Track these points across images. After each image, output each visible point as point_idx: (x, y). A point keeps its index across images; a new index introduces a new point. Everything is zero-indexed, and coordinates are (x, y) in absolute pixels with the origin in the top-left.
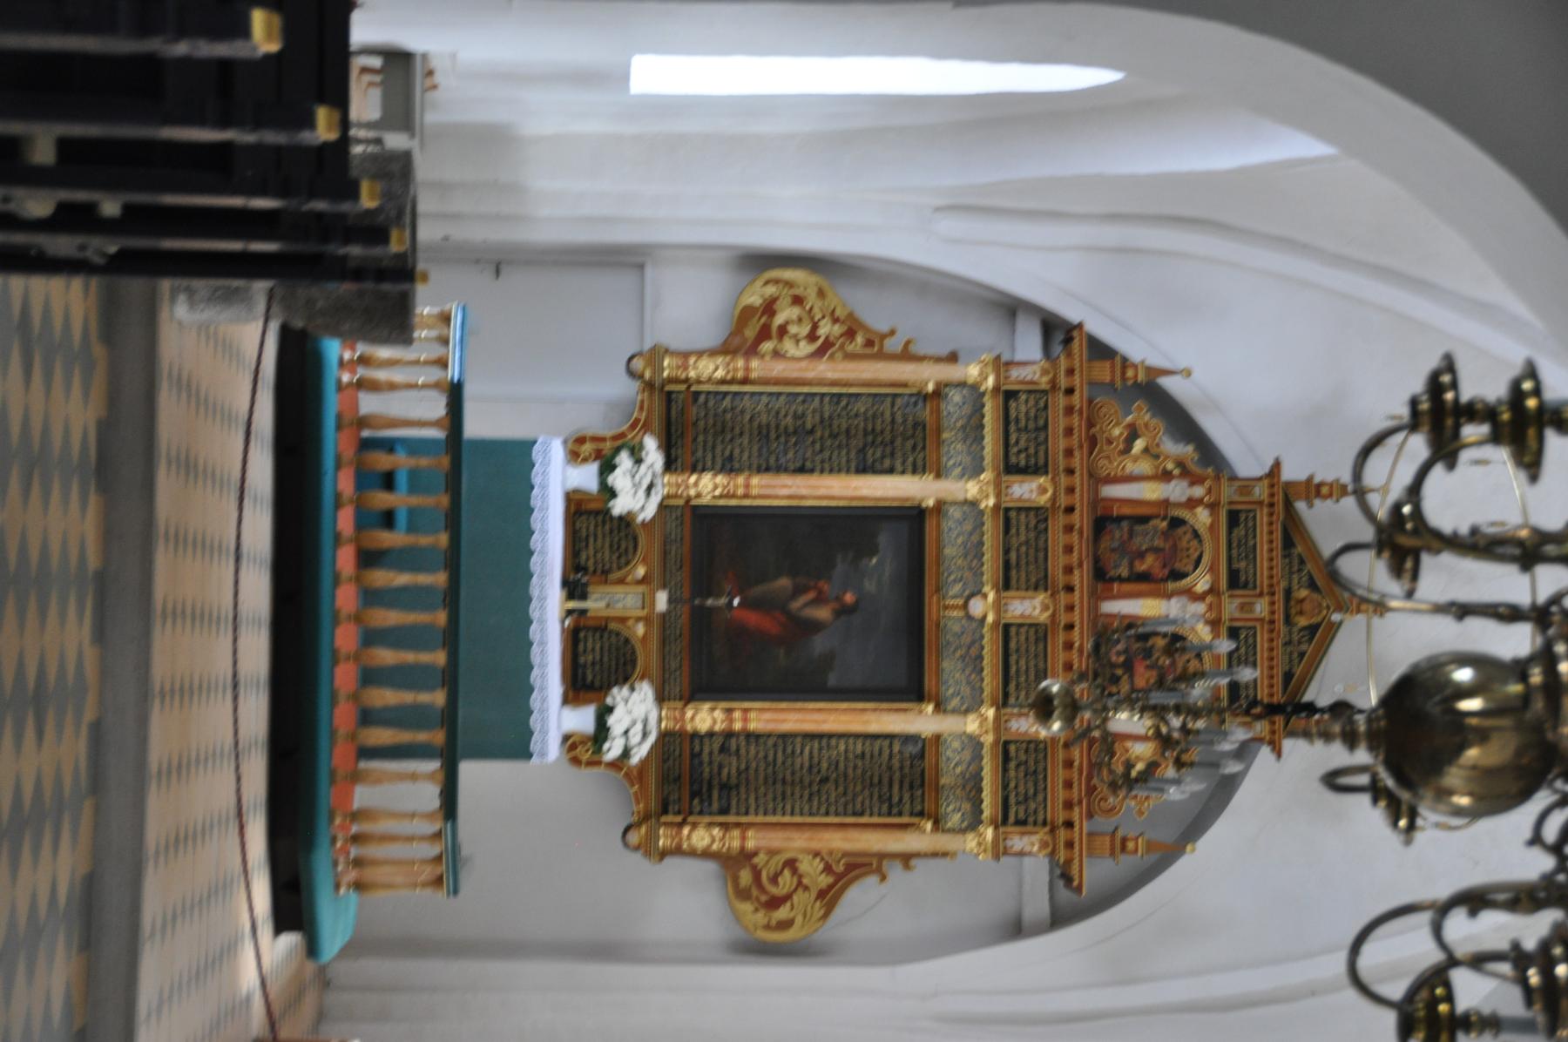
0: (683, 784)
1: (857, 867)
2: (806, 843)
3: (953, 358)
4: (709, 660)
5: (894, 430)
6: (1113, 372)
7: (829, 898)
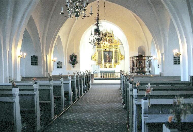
0: (116, 62)
1: (121, 54)
2: (119, 56)
3: (96, 50)
4: (110, 61)
5: (100, 53)
6: (72, 104)
7: (122, 55)
